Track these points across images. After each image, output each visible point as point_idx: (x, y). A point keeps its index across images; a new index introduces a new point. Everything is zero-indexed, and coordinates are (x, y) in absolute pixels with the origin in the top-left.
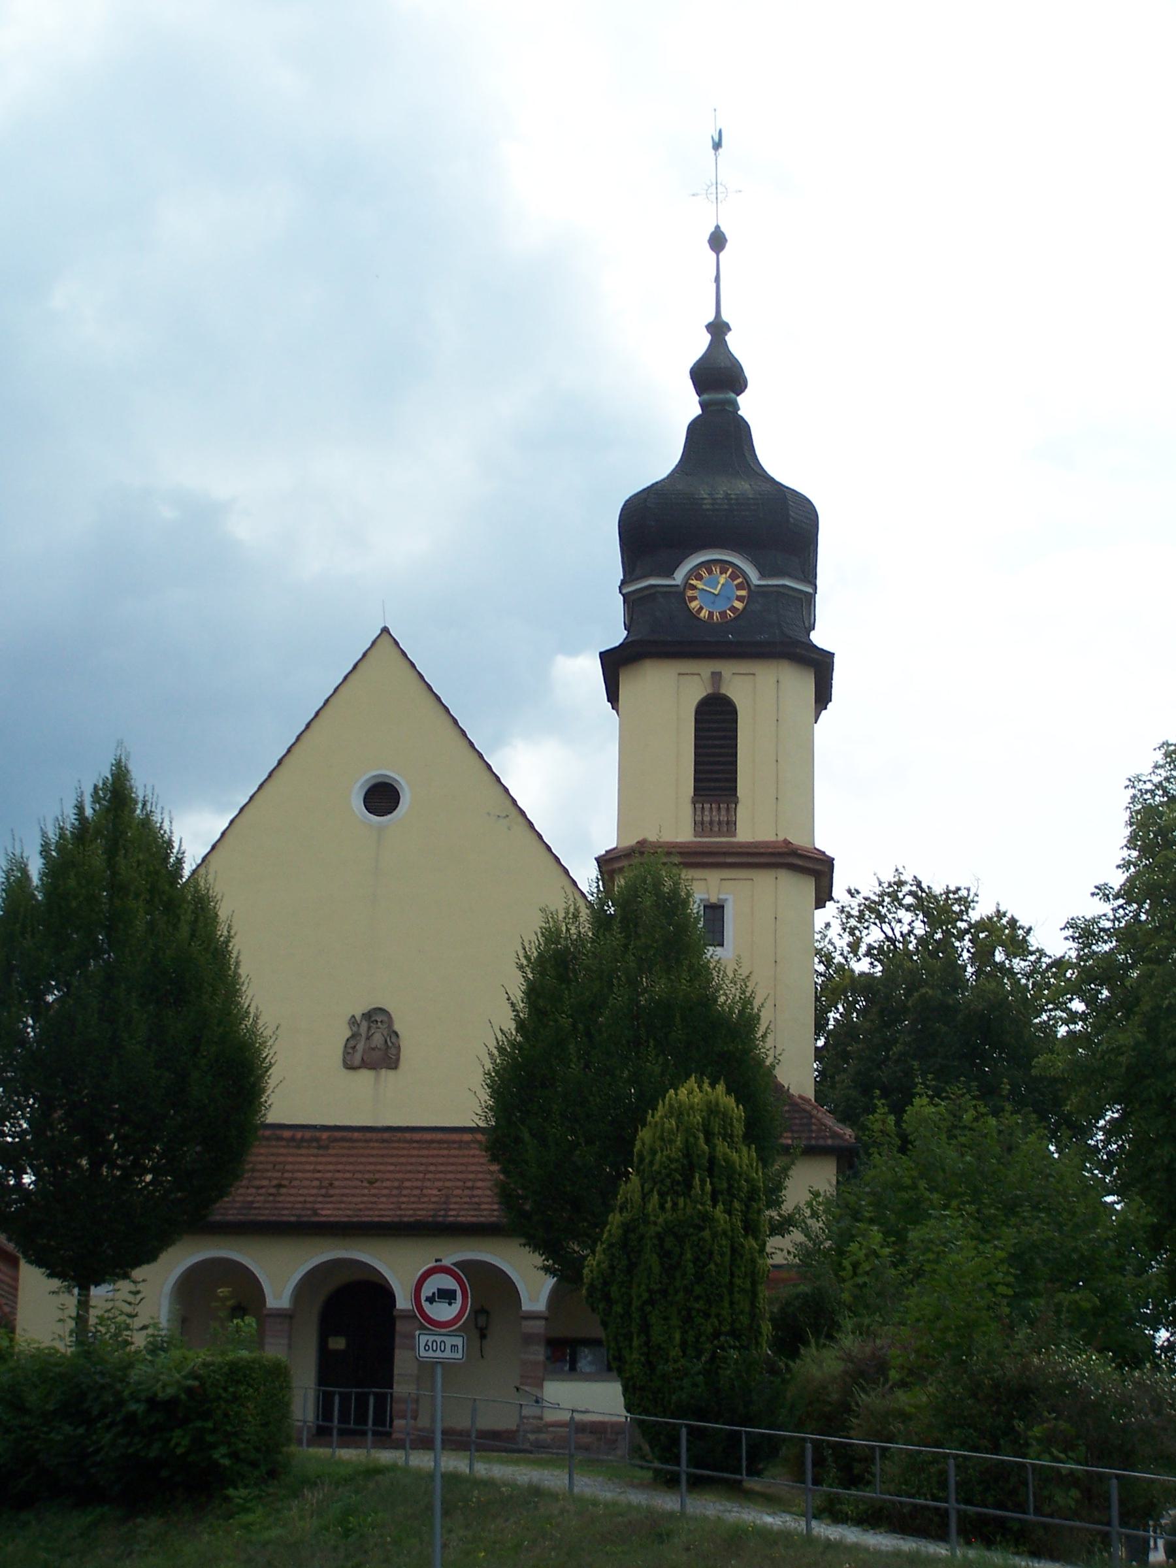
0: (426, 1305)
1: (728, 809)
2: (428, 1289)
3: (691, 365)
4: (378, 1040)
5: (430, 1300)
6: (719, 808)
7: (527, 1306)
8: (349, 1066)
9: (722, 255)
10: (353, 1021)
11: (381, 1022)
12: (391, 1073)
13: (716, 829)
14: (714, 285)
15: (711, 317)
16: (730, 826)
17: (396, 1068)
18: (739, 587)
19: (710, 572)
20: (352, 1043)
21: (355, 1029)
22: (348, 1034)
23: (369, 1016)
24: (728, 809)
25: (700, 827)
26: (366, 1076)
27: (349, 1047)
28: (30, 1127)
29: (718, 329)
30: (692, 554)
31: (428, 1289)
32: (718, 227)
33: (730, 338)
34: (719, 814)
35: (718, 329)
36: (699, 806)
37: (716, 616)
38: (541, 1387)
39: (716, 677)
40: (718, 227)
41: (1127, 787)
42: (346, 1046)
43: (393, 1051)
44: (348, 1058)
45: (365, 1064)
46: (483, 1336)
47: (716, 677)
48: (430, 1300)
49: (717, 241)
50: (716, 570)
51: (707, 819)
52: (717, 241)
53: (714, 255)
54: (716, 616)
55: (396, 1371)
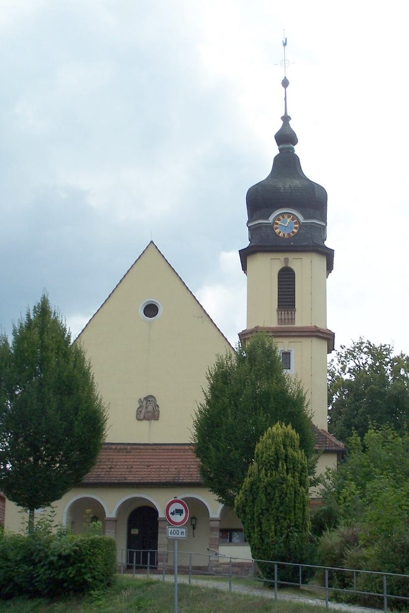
0: (171, 516)
2: (171, 510)
3: (275, 134)
4: (150, 408)
5: (173, 514)
8: (139, 419)
9: (287, 89)
10: (140, 401)
11: (152, 401)
12: (156, 422)
13: (287, 322)
14: (284, 101)
15: (283, 114)
16: (293, 320)
17: (158, 420)
18: (295, 223)
20: (140, 410)
21: (141, 404)
22: (138, 406)
23: (146, 399)
25: (280, 321)
26: (145, 423)
27: (139, 412)
29: (286, 119)
31: (171, 510)
32: (285, 78)
35: (286, 119)
37: (286, 235)
38: (218, 548)
39: (286, 260)
40: (285, 78)
42: (137, 411)
43: (156, 413)
44: (138, 415)
45: (145, 418)
46: (194, 528)
47: (286, 260)
48: (173, 514)
49: (285, 83)
50: (286, 216)
51: (287, 317)
52: (285, 83)
53: (284, 89)
54: (286, 235)
55: (159, 543)
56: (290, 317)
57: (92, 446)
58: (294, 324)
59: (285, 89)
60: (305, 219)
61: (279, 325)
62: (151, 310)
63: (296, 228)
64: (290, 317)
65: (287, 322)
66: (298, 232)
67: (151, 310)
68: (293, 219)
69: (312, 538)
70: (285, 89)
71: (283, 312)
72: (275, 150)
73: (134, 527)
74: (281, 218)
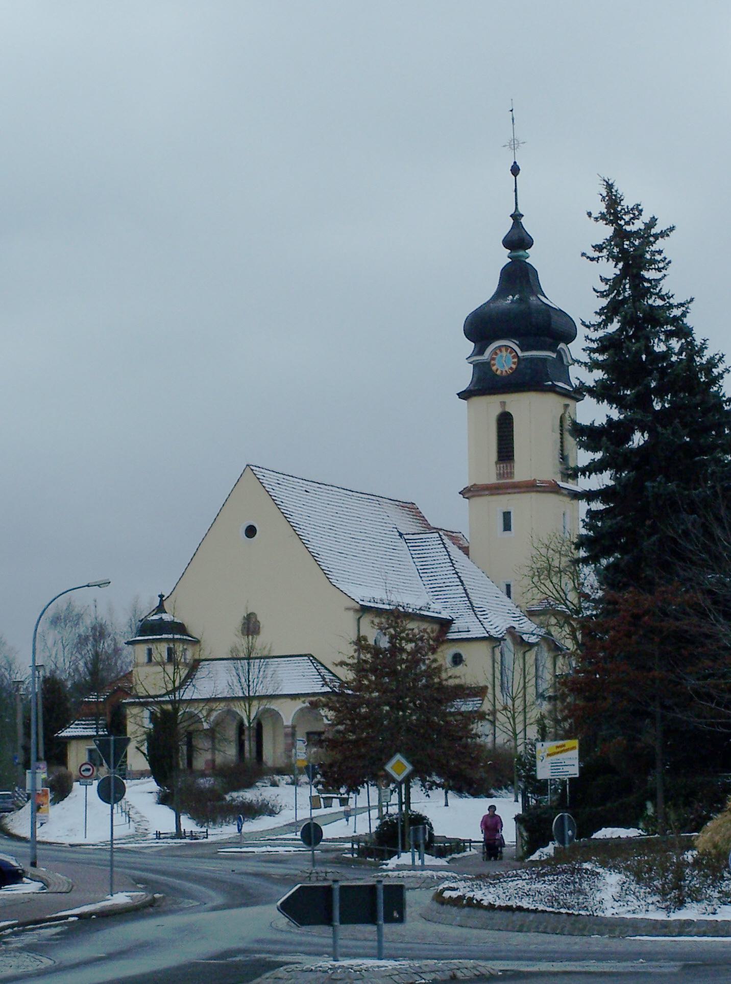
0: (82, 773)
1: (511, 466)
2: (83, 768)
3: (503, 238)
5: (84, 771)
6: (507, 466)
7: (285, 724)
9: (518, 177)
13: (506, 476)
14: (514, 193)
15: (512, 212)
16: (511, 474)
18: (513, 357)
19: (501, 351)
24: (511, 466)
25: (500, 476)
28: (632, 451)
29: (517, 217)
30: (491, 344)
31: (83, 768)
32: (515, 163)
33: (523, 220)
34: (507, 469)
35: (517, 217)
36: (498, 466)
37: (504, 373)
39: (503, 404)
40: (515, 163)
41: (250, 626)
47: (503, 404)
48: (84, 771)
49: (515, 170)
50: (503, 349)
51: (505, 471)
52: (515, 170)
53: (514, 177)
54: (504, 373)
56: (509, 471)
57: (351, 747)
58: (512, 477)
59: (515, 177)
60: (522, 350)
61: (498, 479)
62: (251, 531)
63: (514, 363)
64: (509, 471)
65: (506, 476)
66: (516, 368)
67: (251, 531)
68: (511, 353)
69: (725, 679)
70: (515, 177)
71: (505, 465)
72: (503, 257)
73: (638, 824)
74: (498, 351)
